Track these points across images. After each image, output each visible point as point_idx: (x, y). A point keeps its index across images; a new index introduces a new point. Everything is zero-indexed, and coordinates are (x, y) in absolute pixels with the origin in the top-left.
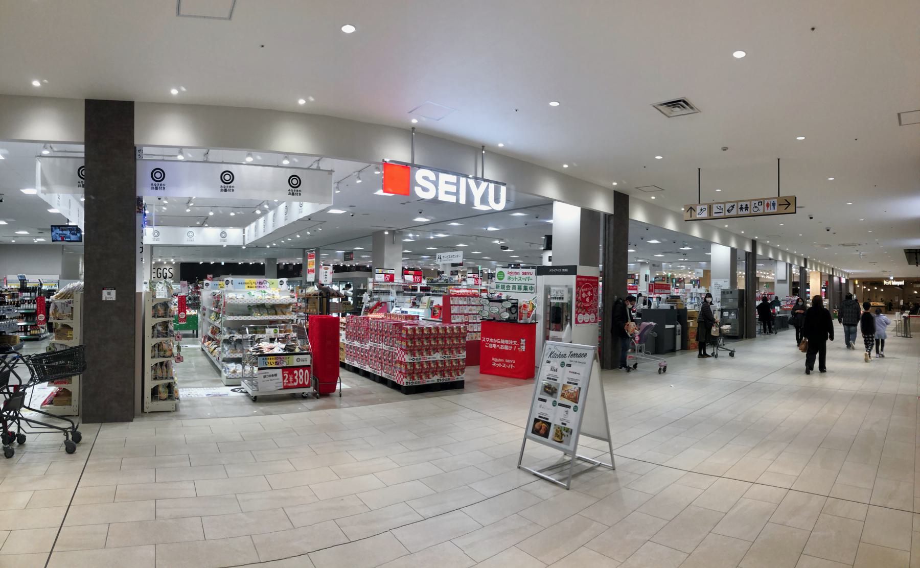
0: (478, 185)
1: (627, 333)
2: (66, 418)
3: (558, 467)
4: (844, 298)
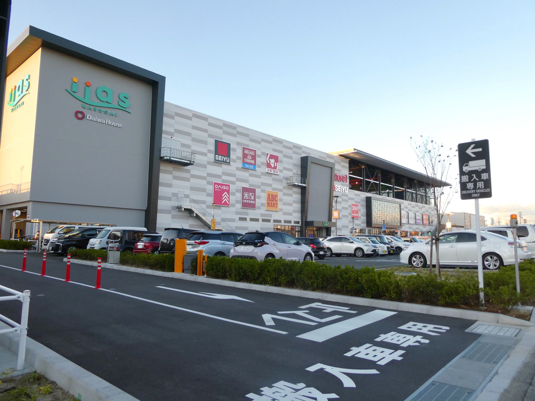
0: (225, 158)
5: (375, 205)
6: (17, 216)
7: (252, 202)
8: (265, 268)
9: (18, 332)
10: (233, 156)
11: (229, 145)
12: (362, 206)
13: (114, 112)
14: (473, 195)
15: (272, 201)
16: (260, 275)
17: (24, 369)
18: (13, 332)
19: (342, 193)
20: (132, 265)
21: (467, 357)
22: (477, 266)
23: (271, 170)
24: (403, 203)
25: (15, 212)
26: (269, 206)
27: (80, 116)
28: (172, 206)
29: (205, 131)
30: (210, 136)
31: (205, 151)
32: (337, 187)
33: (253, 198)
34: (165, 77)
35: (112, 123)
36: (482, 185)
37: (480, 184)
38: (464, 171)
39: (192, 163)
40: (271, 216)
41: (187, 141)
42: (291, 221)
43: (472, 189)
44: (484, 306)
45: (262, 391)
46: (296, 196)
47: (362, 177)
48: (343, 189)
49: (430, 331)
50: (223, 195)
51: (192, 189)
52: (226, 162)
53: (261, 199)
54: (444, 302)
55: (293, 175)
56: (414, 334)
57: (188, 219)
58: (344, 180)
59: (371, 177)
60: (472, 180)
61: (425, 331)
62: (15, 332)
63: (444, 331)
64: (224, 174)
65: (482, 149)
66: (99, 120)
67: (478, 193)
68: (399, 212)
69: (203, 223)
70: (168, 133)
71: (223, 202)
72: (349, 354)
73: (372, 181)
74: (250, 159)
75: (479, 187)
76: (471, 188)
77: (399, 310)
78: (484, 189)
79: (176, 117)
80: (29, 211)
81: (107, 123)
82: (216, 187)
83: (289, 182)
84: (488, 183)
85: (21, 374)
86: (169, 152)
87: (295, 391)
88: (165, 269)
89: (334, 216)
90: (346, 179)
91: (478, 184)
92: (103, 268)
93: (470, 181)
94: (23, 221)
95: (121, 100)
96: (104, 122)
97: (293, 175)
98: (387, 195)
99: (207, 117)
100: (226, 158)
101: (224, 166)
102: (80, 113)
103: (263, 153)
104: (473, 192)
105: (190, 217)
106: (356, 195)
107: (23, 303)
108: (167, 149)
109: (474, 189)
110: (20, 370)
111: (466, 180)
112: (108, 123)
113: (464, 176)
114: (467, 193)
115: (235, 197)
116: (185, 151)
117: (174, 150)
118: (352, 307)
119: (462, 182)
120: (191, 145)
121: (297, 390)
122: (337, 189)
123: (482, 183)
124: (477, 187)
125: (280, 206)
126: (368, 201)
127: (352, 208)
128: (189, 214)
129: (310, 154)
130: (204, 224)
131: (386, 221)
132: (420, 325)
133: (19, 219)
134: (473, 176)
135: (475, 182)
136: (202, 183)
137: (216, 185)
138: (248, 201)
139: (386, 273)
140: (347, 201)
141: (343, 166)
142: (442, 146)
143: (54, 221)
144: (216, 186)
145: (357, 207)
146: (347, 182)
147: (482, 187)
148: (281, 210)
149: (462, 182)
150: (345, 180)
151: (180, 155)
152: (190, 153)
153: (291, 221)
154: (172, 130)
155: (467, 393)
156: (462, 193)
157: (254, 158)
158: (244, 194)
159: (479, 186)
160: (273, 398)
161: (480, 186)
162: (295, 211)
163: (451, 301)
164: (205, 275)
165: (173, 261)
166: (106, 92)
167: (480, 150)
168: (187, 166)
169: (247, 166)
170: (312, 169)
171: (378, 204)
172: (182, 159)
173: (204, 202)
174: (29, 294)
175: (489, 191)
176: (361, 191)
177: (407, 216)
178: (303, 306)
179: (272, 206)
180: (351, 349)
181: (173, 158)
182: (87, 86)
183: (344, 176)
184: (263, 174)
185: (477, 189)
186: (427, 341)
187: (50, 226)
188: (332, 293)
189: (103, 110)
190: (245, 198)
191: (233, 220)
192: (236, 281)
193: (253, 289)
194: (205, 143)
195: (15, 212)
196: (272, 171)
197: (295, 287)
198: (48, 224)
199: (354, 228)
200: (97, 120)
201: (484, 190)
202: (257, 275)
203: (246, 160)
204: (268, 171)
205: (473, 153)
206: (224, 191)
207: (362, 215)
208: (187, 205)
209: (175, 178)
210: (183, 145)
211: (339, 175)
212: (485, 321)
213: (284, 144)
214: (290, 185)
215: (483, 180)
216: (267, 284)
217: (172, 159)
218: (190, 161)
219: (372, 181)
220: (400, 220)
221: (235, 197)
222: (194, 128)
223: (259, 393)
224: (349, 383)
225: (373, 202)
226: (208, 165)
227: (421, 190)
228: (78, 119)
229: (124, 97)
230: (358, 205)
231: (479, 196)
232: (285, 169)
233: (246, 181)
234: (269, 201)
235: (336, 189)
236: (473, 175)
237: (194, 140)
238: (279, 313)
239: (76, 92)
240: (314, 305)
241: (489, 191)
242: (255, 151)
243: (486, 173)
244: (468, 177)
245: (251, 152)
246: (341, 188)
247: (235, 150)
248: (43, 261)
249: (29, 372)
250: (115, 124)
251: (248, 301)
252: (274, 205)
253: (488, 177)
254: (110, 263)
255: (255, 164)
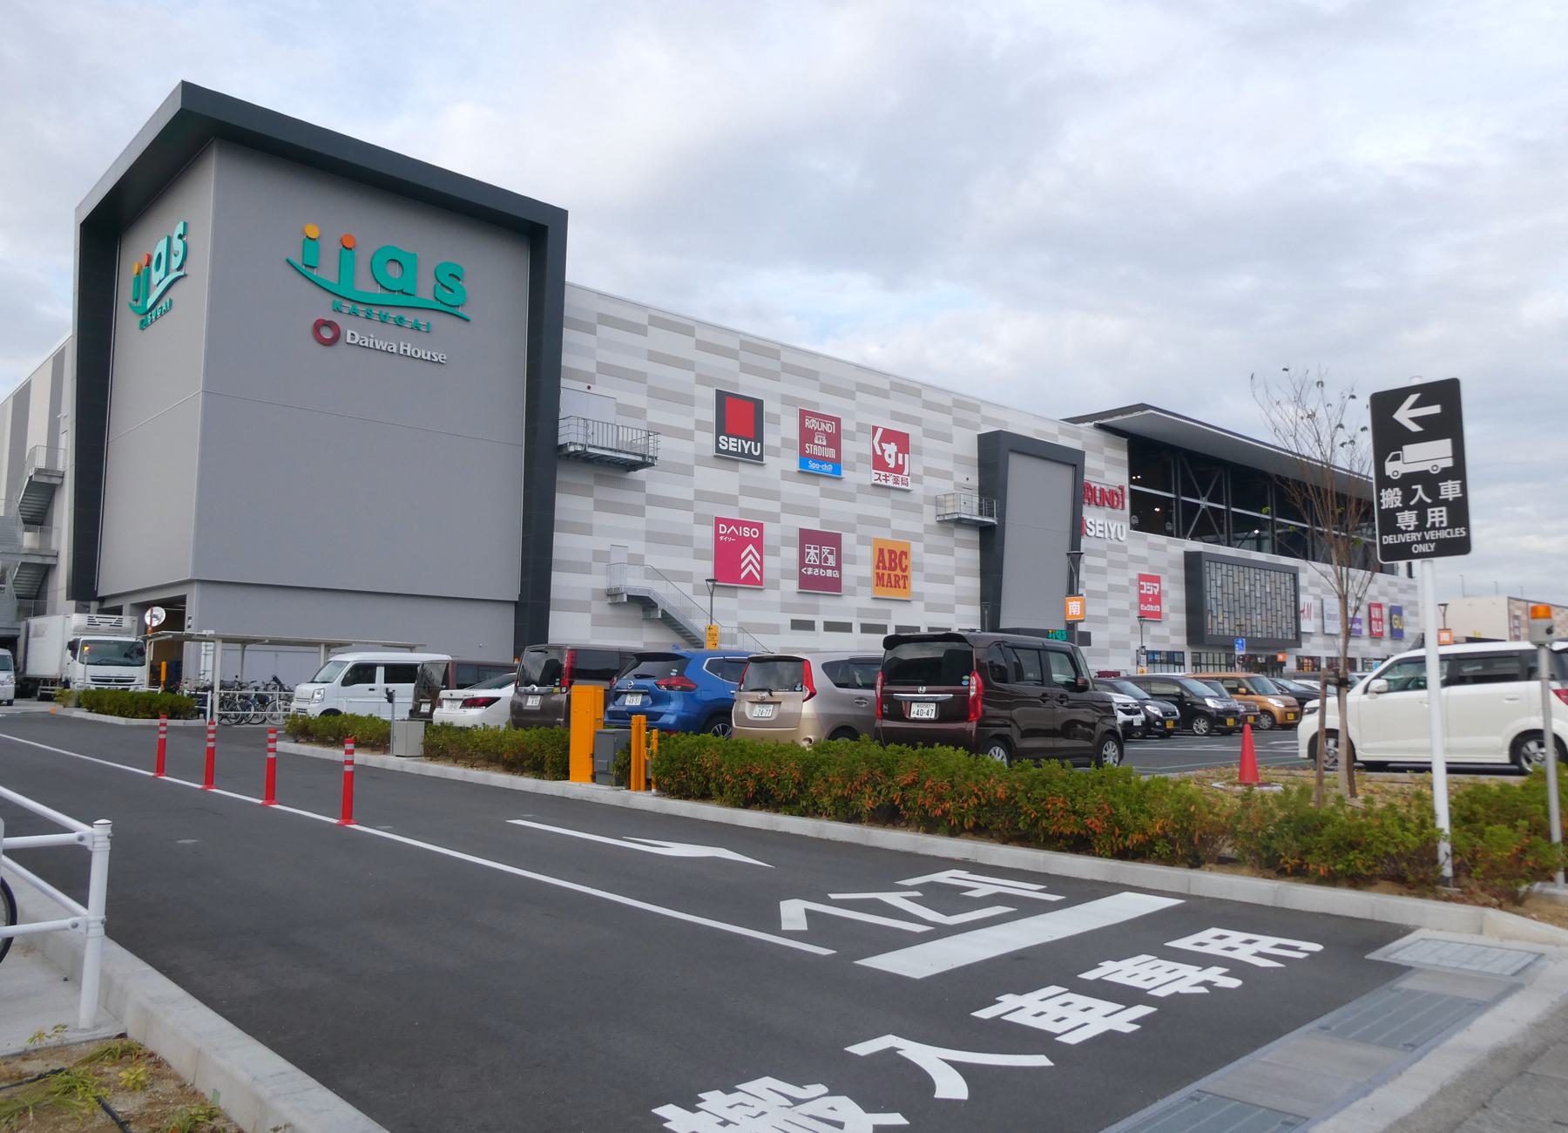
0: (746, 443)
5: (1216, 581)
6: (155, 623)
7: (829, 573)
8: (817, 769)
9: (81, 929)
10: (771, 437)
11: (758, 404)
12: (1172, 580)
13: (423, 318)
14: (1416, 549)
15: (891, 569)
16: (802, 787)
17: (97, 1027)
18: (66, 929)
19: (1109, 541)
20: (455, 762)
21: (1334, 1028)
22: (1430, 763)
23: (885, 476)
24: (1305, 571)
25: (152, 612)
26: (883, 586)
27: (327, 334)
28: (593, 589)
29: (687, 365)
30: (702, 380)
31: (688, 424)
32: (1091, 523)
33: (832, 561)
34: (565, 213)
35: (416, 352)
36: (1441, 516)
37: (1437, 514)
38: (1389, 476)
39: (650, 460)
40: (888, 614)
41: (634, 397)
42: (826, 629)
43: (1412, 528)
44: (1451, 885)
45: (702, 1100)
46: (968, 555)
47: (1170, 492)
48: (1113, 530)
49: (1260, 954)
50: (743, 556)
51: (653, 537)
52: (750, 455)
53: (858, 567)
54: (1326, 869)
55: (955, 489)
56: (1204, 961)
57: (642, 628)
58: (1116, 503)
59: (1208, 494)
60: (1412, 503)
61: (1245, 954)
62: (72, 930)
63: (1301, 955)
64: (747, 491)
65: (1443, 408)
66: (381, 343)
67: (1431, 541)
68: (1293, 598)
69: (683, 637)
70: (577, 375)
71: (743, 576)
72: (985, 1014)
73: (1203, 503)
74: (822, 446)
75: (1434, 523)
76: (1409, 526)
77: (1193, 892)
78: (1448, 530)
79: (599, 327)
80: (191, 609)
81: (402, 352)
82: (721, 532)
83: (942, 511)
84: (1459, 512)
85: (88, 1039)
86: (581, 430)
87: (791, 1104)
88: (543, 771)
89: (1070, 614)
90: (1121, 500)
91: (1430, 515)
92: (363, 767)
93: (1406, 506)
94: (171, 636)
95: (442, 284)
96: (395, 350)
97: (955, 489)
98: (1255, 546)
99: (693, 324)
100: (749, 443)
101: (746, 471)
102: (326, 325)
103: (861, 427)
104: (1417, 537)
105: (644, 622)
106: (1151, 546)
107: (93, 854)
108: (575, 422)
109: (1418, 529)
110: (84, 1030)
111: (1394, 503)
112: (405, 351)
113: (1389, 490)
114: (1399, 541)
115: (781, 561)
116: (628, 428)
117: (596, 423)
118: (1051, 882)
119: (1383, 508)
120: (645, 410)
121: (797, 1102)
122: (1091, 530)
123: (1441, 511)
124: (1426, 523)
125: (917, 584)
126: (1193, 563)
127: (1142, 587)
128: (643, 611)
129: (1006, 423)
130: (687, 640)
131: (1249, 626)
132: (1236, 937)
133: (160, 633)
134: (1417, 490)
135: (1421, 508)
136: (681, 519)
137: (721, 525)
138: (817, 570)
139: (1164, 784)
140: (1123, 566)
141: (1109, 460)
142: (1353, 397)
143: (256, 636)
144: (723, 528)
145: (1155, 585)
146: (1123, 508)
147: (1441, 522)
148: (920, 597)
149: (1383, 508)
150: (1118, 501)
151: (615, 438)
152: (644, 432)
153: (826, 629)
154: (589, 366)
155: (1279, 1125)
156: (1384, 543)
157: (834, 441)
158: (807, 550)
159: (1433, 520)
160: (725, 1120)
161: (1437, 520)
162: (961, 600)
163: (1345, 867)
164: (653, 790)
165: (567, 748)
166: (399, 263)
167: (1435, 409)
168: (635, 470)
169: (813, 466)
170: (1019, 470)
171: (1224, 573)
172: (620, 451)
173: (685, 577)
174: (108, 831)
175: (1464, 534)
176: (1170, 534)
177: (1319, 611)
178: (907, 881)
179: (891, 586)
180: (998, 999)
181: (594, 447)
182: (346, 248)
183: (1114, 489)
184: (861, 488)
185: (1428, 530)
186: (1234, 983)
187: (246, 653)
188: (1006, 841)
189: (393, 313)
190: (810, 561)
191: (773, 629)
192: (735, 805)
193: (782, 829)
194: (688, 400)
195: (152, 612)
196: (891, 478)
197: (903, 824)
198: (239, 646)
199: (1143, 650)
200: (374, 343)
201: (1449, 533)
202: (794, 791)
203: (809, 447)
204: (879, 478)
205: (1415, 420)
206: (743, 542)
207: (1173, 609)
208: (635, 582)
209: (600, 506)
210: (623, 410)
211: (1098, 488)
212: (1442, 930)
213: (927, 395)
214: (946, 521)
215: (1445, 502)
216: (821, 814)
217: (590, 450)
218: (644, 456)
219: (1203, 503)
220: (1294, 623)
221: (781, 561)
222: (654, 357)
223: (690, 1103)
224: (951, 1087)
225: (1207, 569)
226: (696, 467)
227: (1364, 527)
228: (325, 345)
229: (450, 275)
230: (1159, 577)
231: (1432, 550)
232: (929, 471)
233: (813, 512)
234: (881, 571)
235: (1088, 530)
236: (1414, 487)
237: (654, 393)
238: (833, 896)
239: (314, 267)
240: (942, 877)
241: (1464, 534)
242: (838, 421)
243: (1453, 480)
244: (1400, 493)
245: (825, 423)
246: (1104, 526)
247: (776, 419)
248: (160, 740)
249: (107, 1035)
250: (426, 355)
251: (747, 863)
252: (897, 582)
253: (1442, 488)
254: (397, 756)
255: (837, 461)
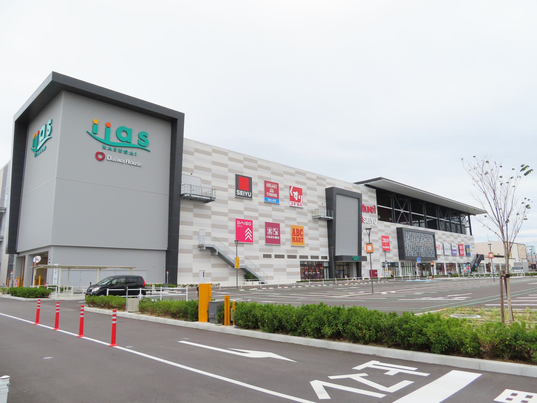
0: (246, 192)
1: (384, 238)
2: (498, 219)
3: (123, 278)
4: (534, 272)
